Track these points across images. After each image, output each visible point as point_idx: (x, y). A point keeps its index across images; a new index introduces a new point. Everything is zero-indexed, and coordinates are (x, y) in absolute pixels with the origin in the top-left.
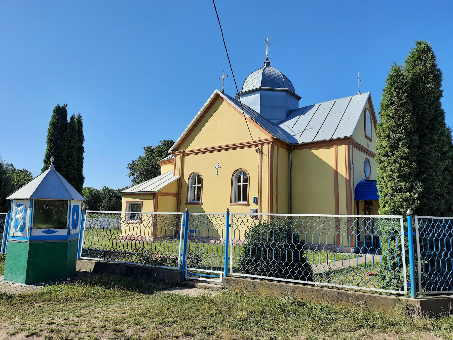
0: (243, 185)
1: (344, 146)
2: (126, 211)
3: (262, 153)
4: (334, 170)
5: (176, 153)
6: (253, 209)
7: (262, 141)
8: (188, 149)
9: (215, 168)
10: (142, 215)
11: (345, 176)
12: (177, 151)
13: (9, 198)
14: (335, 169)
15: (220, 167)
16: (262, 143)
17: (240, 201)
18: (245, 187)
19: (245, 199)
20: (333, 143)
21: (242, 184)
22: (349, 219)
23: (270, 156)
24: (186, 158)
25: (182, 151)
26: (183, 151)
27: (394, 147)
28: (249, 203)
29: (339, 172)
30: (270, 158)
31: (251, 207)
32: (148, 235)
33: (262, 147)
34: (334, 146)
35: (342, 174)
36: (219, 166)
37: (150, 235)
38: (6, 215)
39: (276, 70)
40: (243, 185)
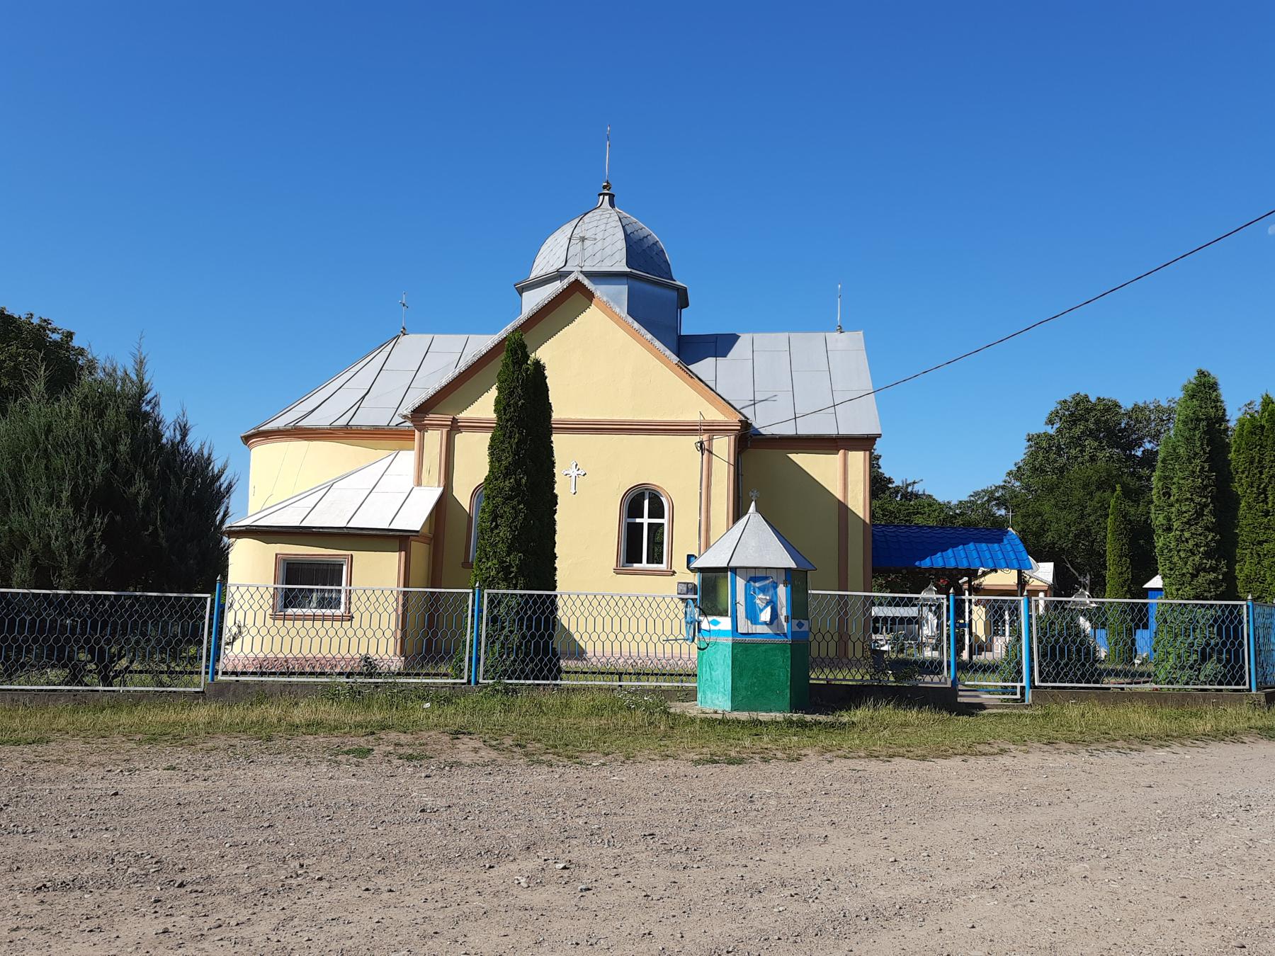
0: (649, 524)
1: (862, 453)
2: (275, 584)
3: (710, 452)
4: (839, 500)
5: (426, 422)
6: (688, 583)
7: (712, 424)
8: (464, 415)
9: (566, 475)
10: (556, 596)
11: (862, 516)
12: (431, 416)
13: (1146, 586)
14: (841, 499)
15: (584, 475)
16: (713, 430)
17: (641, 562)
18: (656, 530)
19: (656, 557)
20: (839, 444)
21: (646, 521)
22: (193, 599)
23: (732, 462)
24: (461, 439)
25: (452, 417)
26: (454, 418)
27: (1199, 514)
28: (673, 569)
29: (849, 506)
30: (732, 468)
31: (677, 579)
32: (320, 651)
33: (710, 440)
34: (842, 452)
35: (856, 511)
36: (579, 472)
37: (391, 652)
38: (206, 598)
39: (624, 213)
40: (649, 524)
